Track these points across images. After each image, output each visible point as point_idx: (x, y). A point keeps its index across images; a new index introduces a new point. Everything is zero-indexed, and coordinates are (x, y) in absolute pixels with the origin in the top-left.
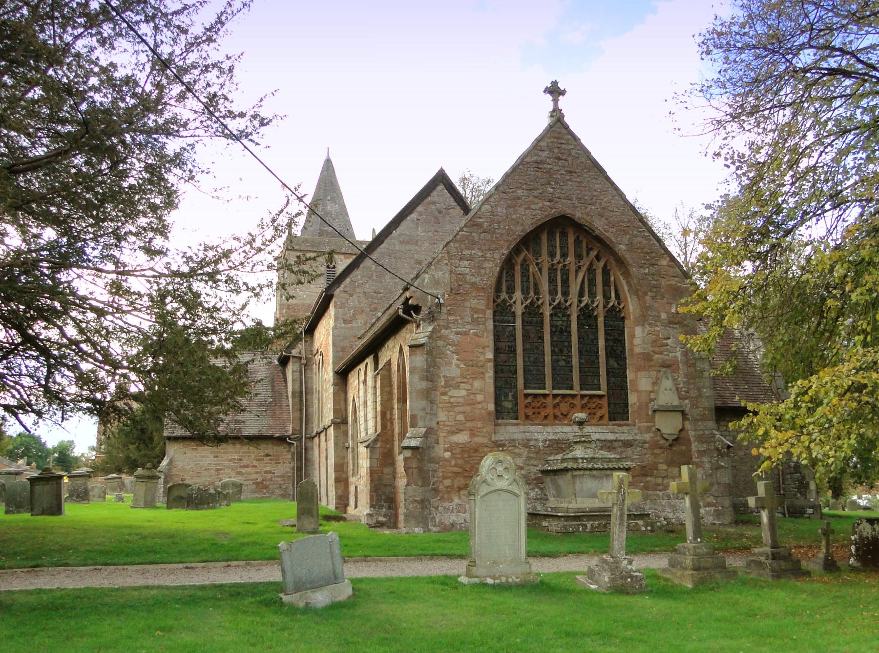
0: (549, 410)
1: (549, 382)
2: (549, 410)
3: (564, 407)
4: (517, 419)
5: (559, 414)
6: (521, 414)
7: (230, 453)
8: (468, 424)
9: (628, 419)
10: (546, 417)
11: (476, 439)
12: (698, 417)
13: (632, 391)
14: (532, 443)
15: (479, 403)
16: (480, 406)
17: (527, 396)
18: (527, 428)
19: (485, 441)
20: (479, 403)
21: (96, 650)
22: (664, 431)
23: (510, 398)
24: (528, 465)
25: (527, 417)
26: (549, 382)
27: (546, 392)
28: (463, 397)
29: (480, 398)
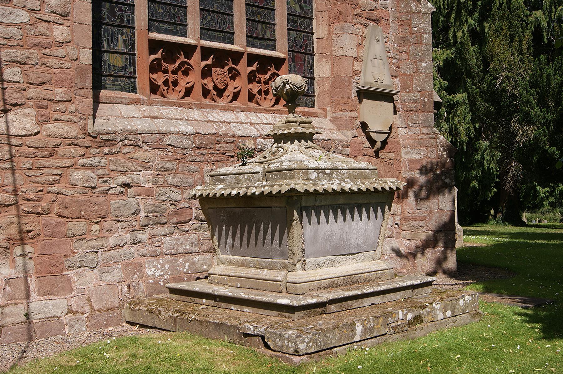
0: (194, 78)
1: (193, 22)
2: (194, 78)
3: (219, 75)
4: (134, 90)
5: (210, 86)
6: (143, 77)
7: (120, 170)
8: (32, 92)
9: (313, 106)
10: (188, 92)
11: (51, 128)
12: (413, 107)
13: (322, 56)
14: (168, 140)
15: (61, 44)
16: (61, 52)
17: (154, 46)
18: (156, 110)
19: (72, 130)
20: (61, 44)
21: (7, 198)
22: (372, 127)
23: (120, 46)
24: (161, 186)
25: (154, 89)
26: (193, 22)
27: (189, 40)
28: (20, 26)
29: (60, 32)
